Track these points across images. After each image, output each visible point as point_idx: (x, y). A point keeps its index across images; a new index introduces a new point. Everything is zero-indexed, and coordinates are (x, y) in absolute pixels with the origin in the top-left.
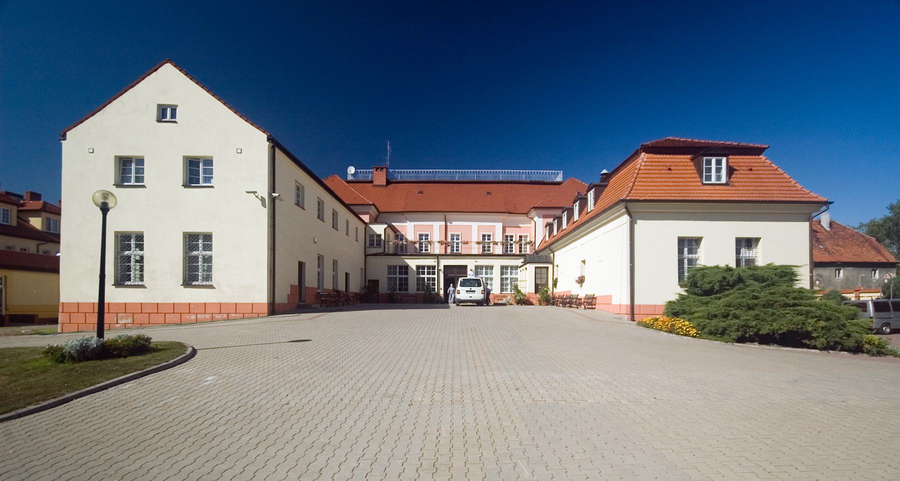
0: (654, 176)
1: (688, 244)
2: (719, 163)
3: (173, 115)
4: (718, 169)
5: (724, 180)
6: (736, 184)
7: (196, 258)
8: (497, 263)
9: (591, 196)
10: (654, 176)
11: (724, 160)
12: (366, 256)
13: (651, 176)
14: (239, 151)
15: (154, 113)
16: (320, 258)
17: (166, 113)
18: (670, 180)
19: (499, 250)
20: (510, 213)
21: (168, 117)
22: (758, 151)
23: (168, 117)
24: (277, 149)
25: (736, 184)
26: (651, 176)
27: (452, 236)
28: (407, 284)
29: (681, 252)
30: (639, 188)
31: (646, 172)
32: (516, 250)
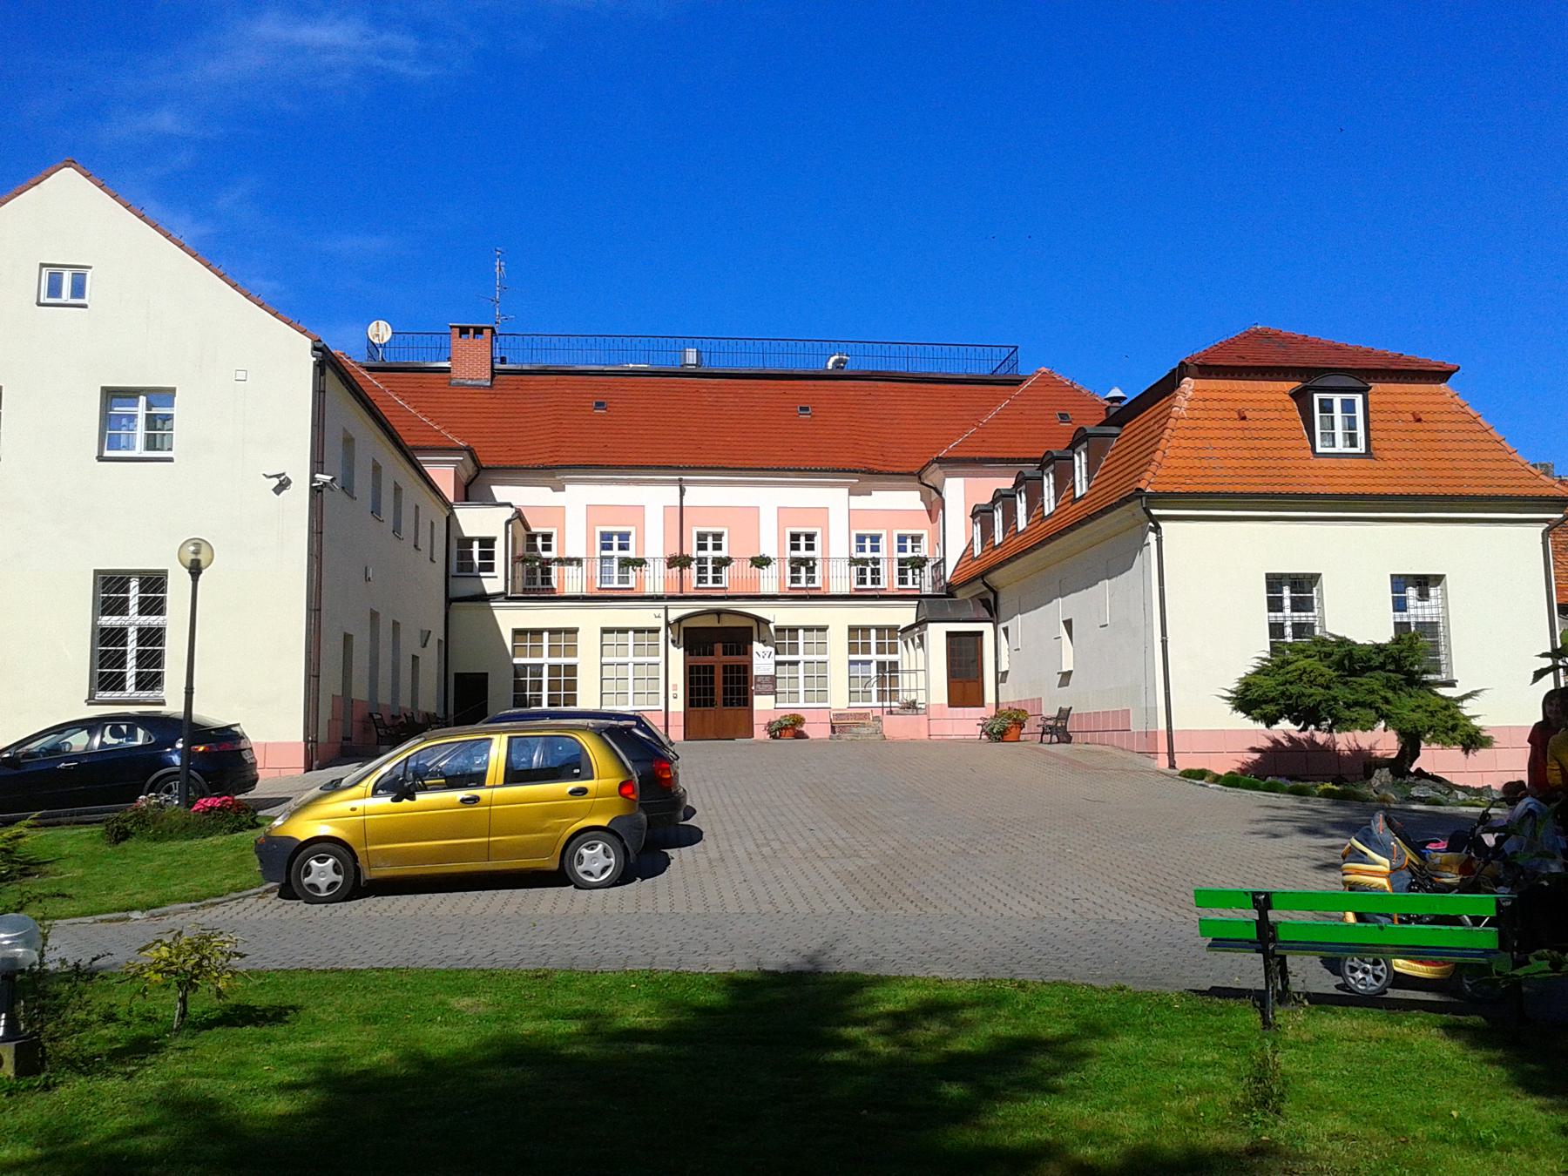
0: (1210, 434)
1: (1291, 589)
2: (1348, 407)
3: (79, 289)
4: (1341, 424)
5: (1361, 448)
6: (1388, 454)
7: (118, 635)
8: (838, 619)
9: (1080, 461)
10: (1210, 434)
11: (1359, 398)
12: (449, 601)
13: (1203, 434)
14: (241, 375)
15: (30, 283)
16: (374, 615)
17: (64, 285)
18: (1243, 444)
19: (841, 580)
20: (870, 472)
21: (66, 295)
22: (1442, 375)
23: (66, 295)
24: (328, 371)
25: (1388, 454)
26: (1203, 434)
27: (702, 537)
28: (572, 685)
29: (1274, 605)
30: (1174, 463)
31: (1192, 423)
32: (889, 579)
